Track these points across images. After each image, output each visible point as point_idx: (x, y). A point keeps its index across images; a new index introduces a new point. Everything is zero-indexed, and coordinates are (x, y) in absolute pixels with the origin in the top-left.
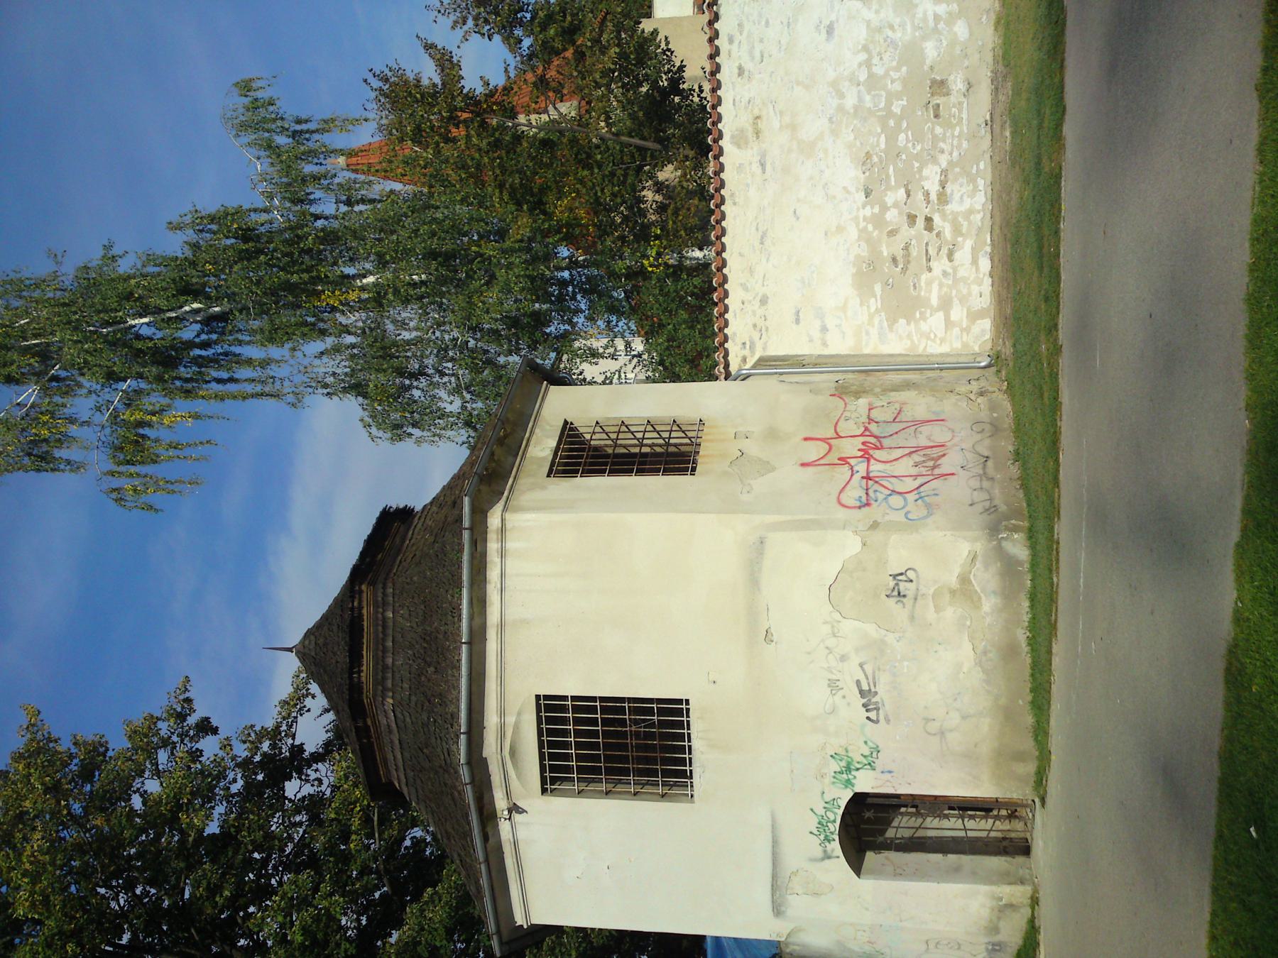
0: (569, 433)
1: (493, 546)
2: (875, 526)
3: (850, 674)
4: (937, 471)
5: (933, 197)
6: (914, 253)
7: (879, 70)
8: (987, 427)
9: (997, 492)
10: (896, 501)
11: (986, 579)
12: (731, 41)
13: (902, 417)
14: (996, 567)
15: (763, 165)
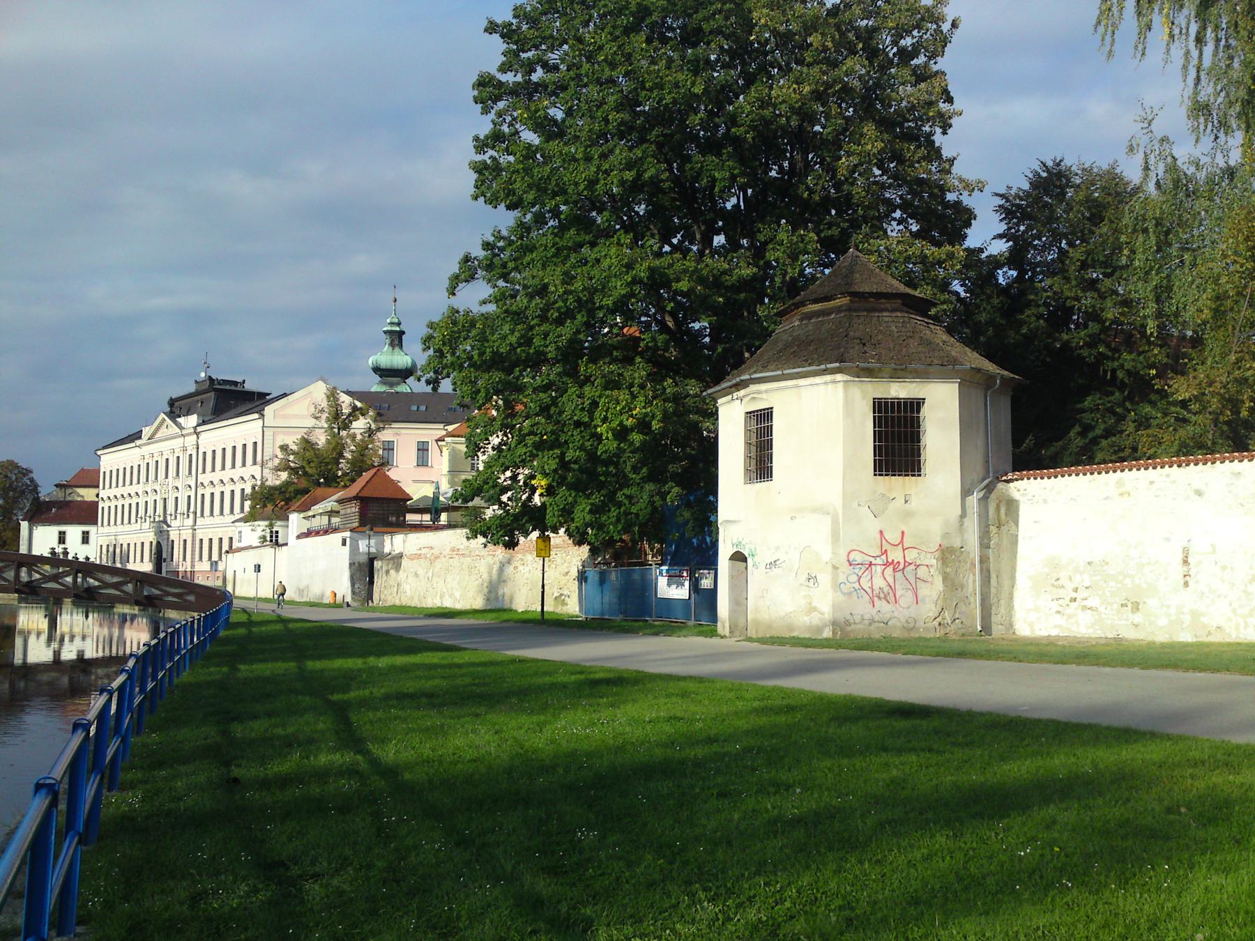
0: (915, 405)
2: (835, 568)
4: (876, 599)
6: (1061, 591)
9: (861, 626)
10: (854, 578)
11: (815, 619)
12: (1168, 476)
13: (920, 584)
14: (819, 623)
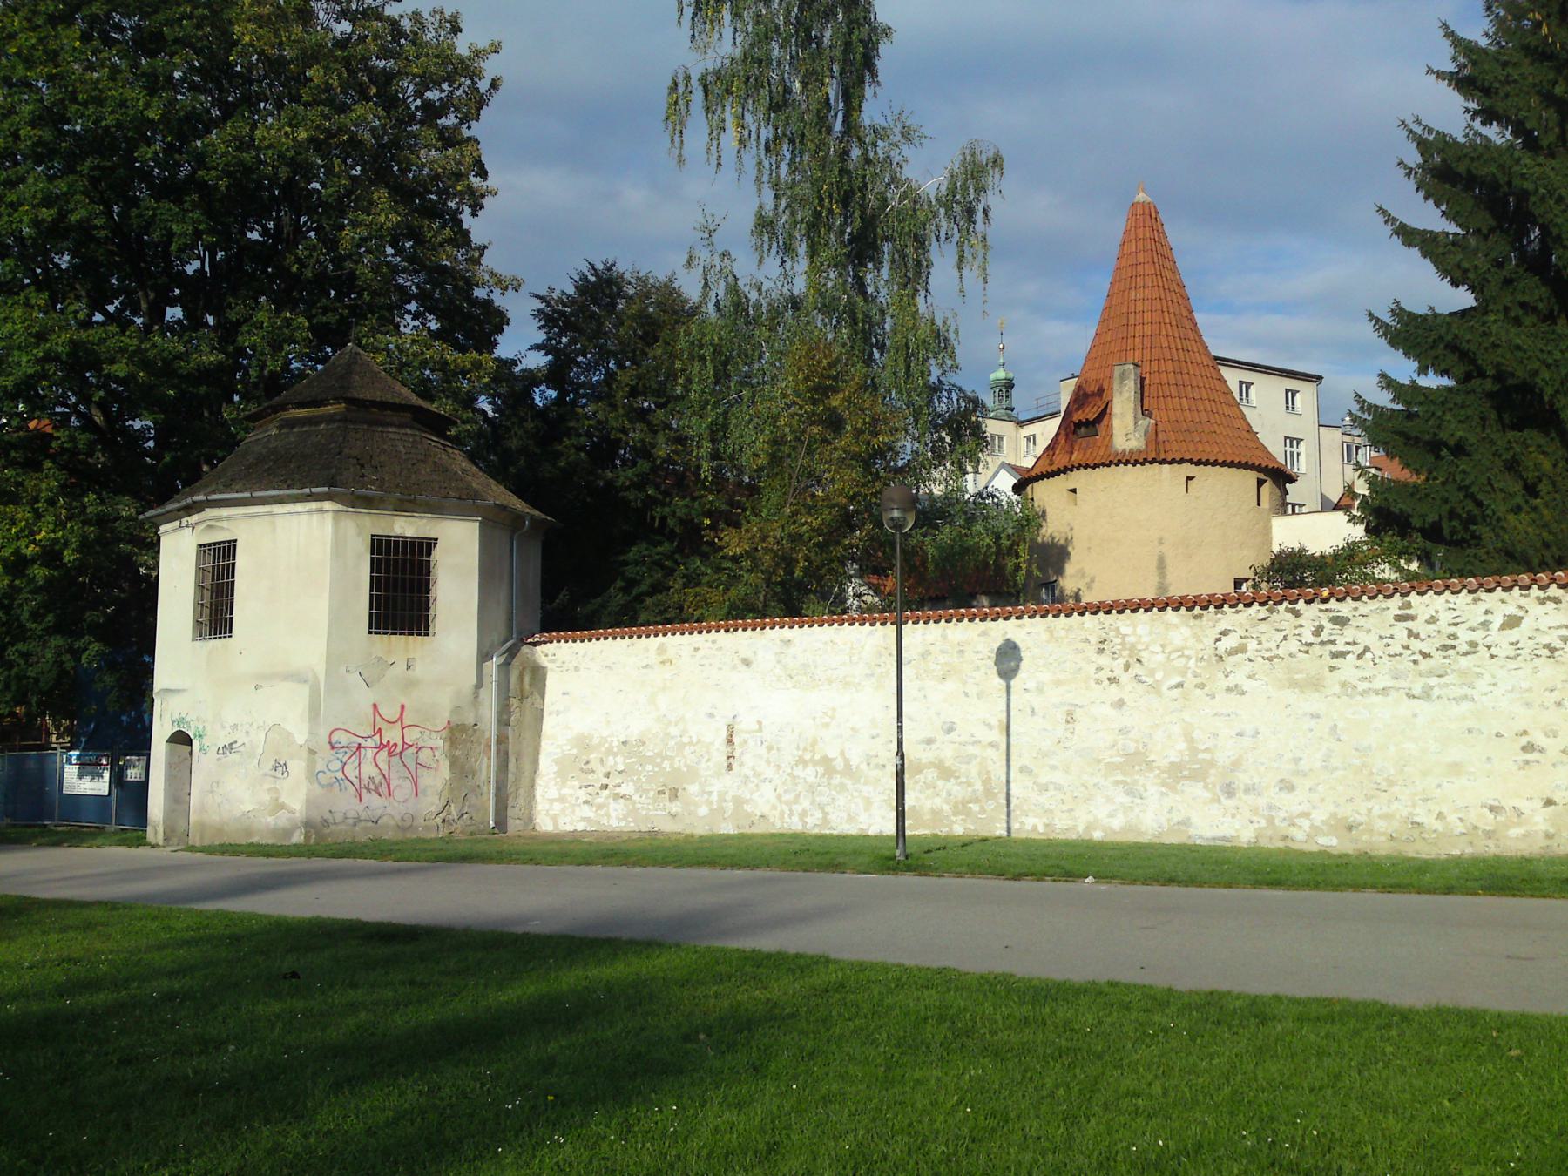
0: (425, 547)
1: (314, 505)
2: (312, 752)
3: (240, 737)
4: (364, 791)
5: (618, 790)
7: (687, 750)
8: (408, 824)
9: (343, 827)
10: (338, 765)
11: (282, 820)
12: (714, 642)
15: (646, 667)
